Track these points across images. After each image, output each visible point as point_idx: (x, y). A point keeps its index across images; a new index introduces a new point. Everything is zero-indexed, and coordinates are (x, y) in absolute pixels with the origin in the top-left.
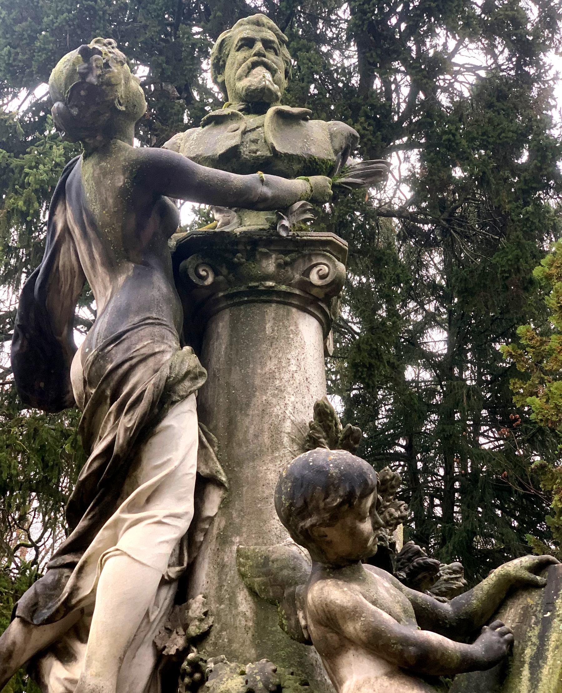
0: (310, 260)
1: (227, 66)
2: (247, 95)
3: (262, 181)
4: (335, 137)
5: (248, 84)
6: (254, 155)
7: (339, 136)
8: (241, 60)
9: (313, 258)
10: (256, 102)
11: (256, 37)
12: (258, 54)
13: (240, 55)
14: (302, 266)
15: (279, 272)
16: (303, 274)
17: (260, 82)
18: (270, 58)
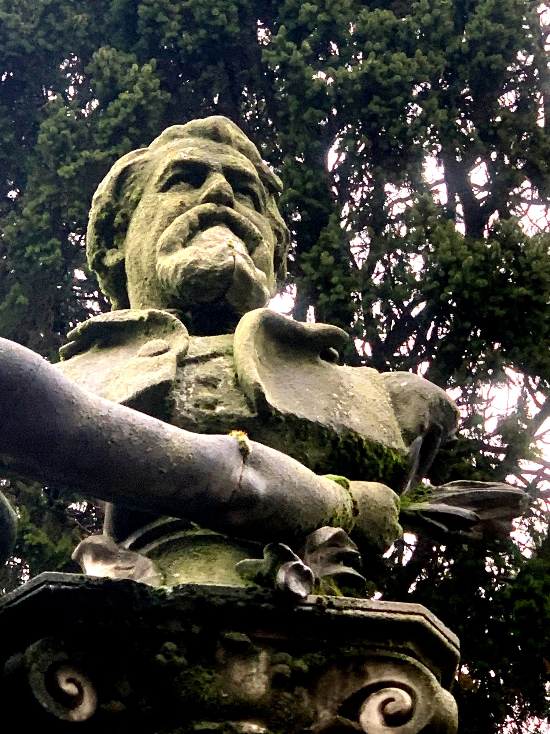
0: (364, 675)
1: (132, 225)
2: (185, 284)
3: (244, 452)
4: (406, 402)
5: (191, 259)
6: (208, 412)
7: (415, 401)
8: (172, 209)
9: (370, 669)
10: (210, 303)
11: (213, 163)
12: (216, 197)
13: (171, 200)
14: (340, 690)
15: (276, 698)
16: (341, 711)
17: (221, 256)
18: (243, 211)
